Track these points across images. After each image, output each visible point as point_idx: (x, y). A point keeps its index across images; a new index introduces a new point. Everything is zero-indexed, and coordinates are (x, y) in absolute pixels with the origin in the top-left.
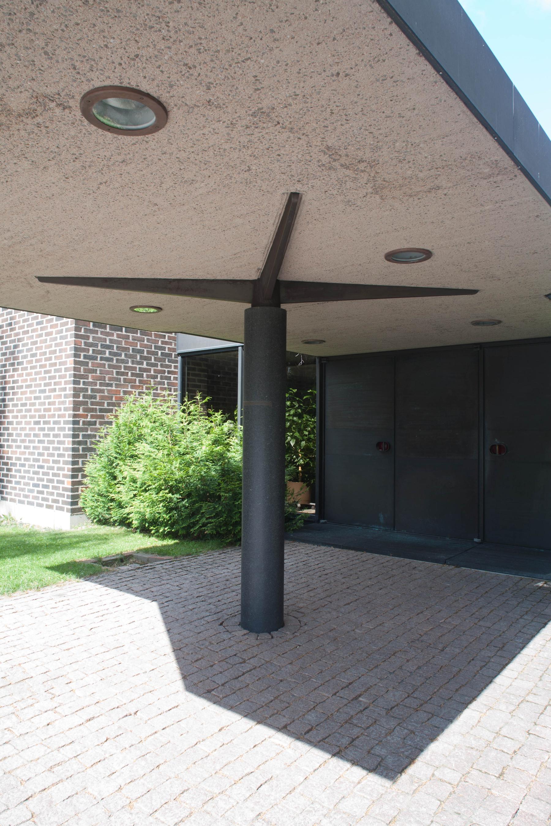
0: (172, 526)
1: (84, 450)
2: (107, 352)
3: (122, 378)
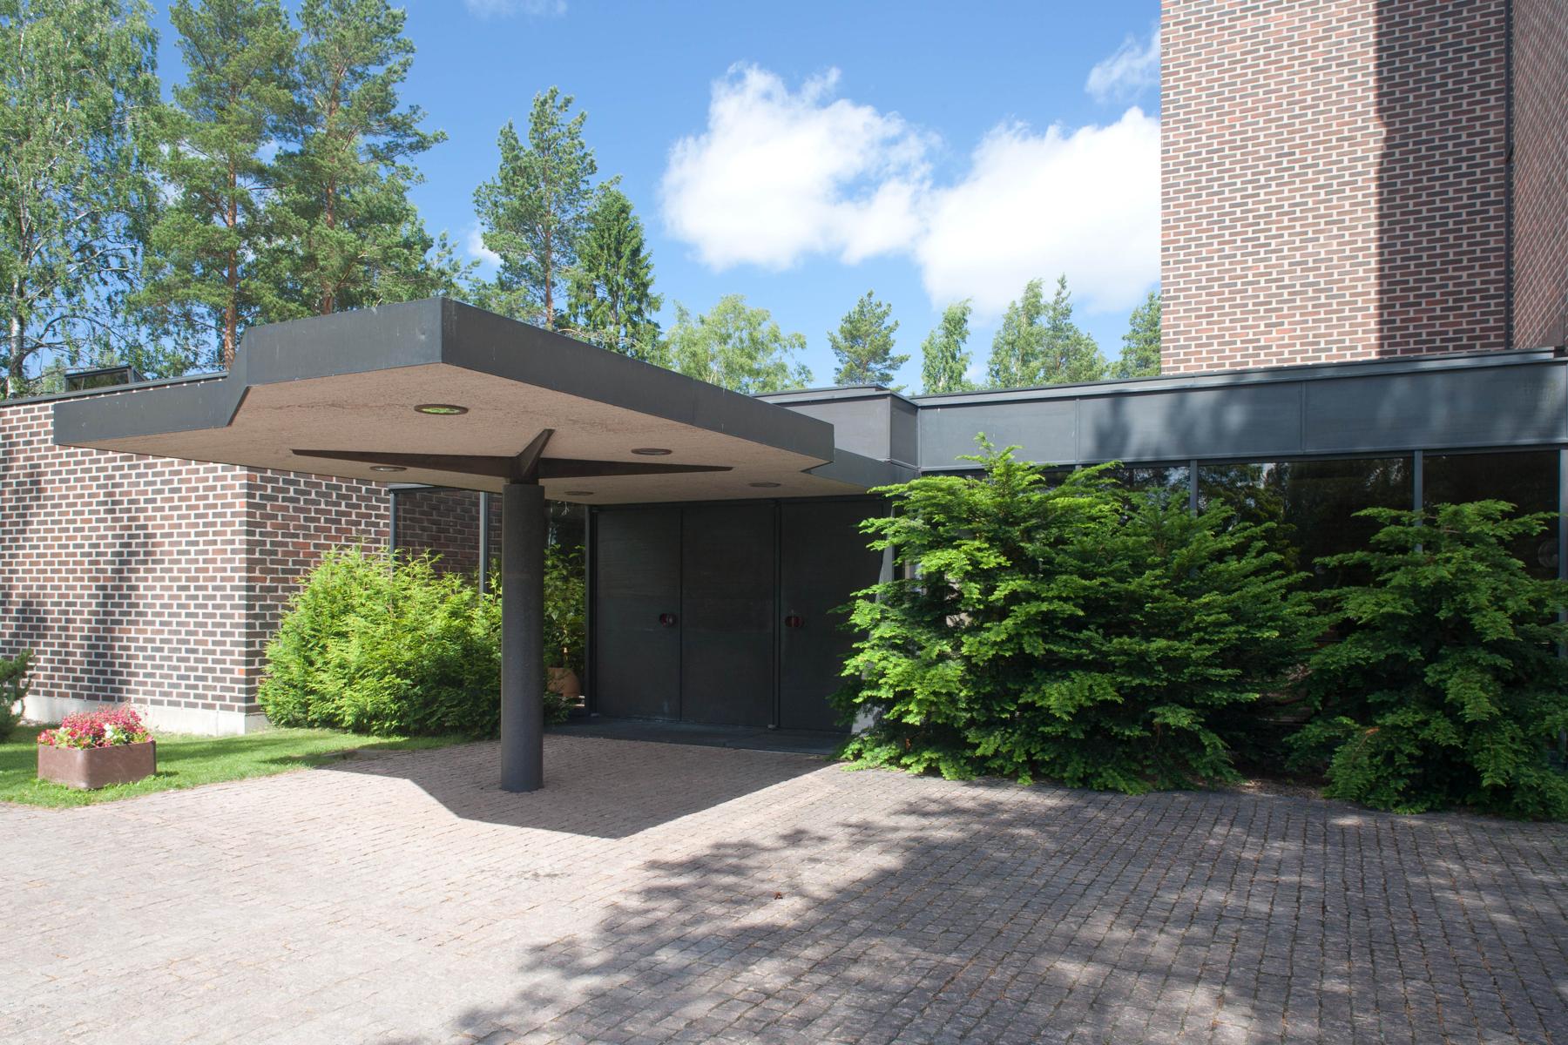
0: (401, 719)
1: (262, 626)
2: (292, 489)
3: (312, 525)
